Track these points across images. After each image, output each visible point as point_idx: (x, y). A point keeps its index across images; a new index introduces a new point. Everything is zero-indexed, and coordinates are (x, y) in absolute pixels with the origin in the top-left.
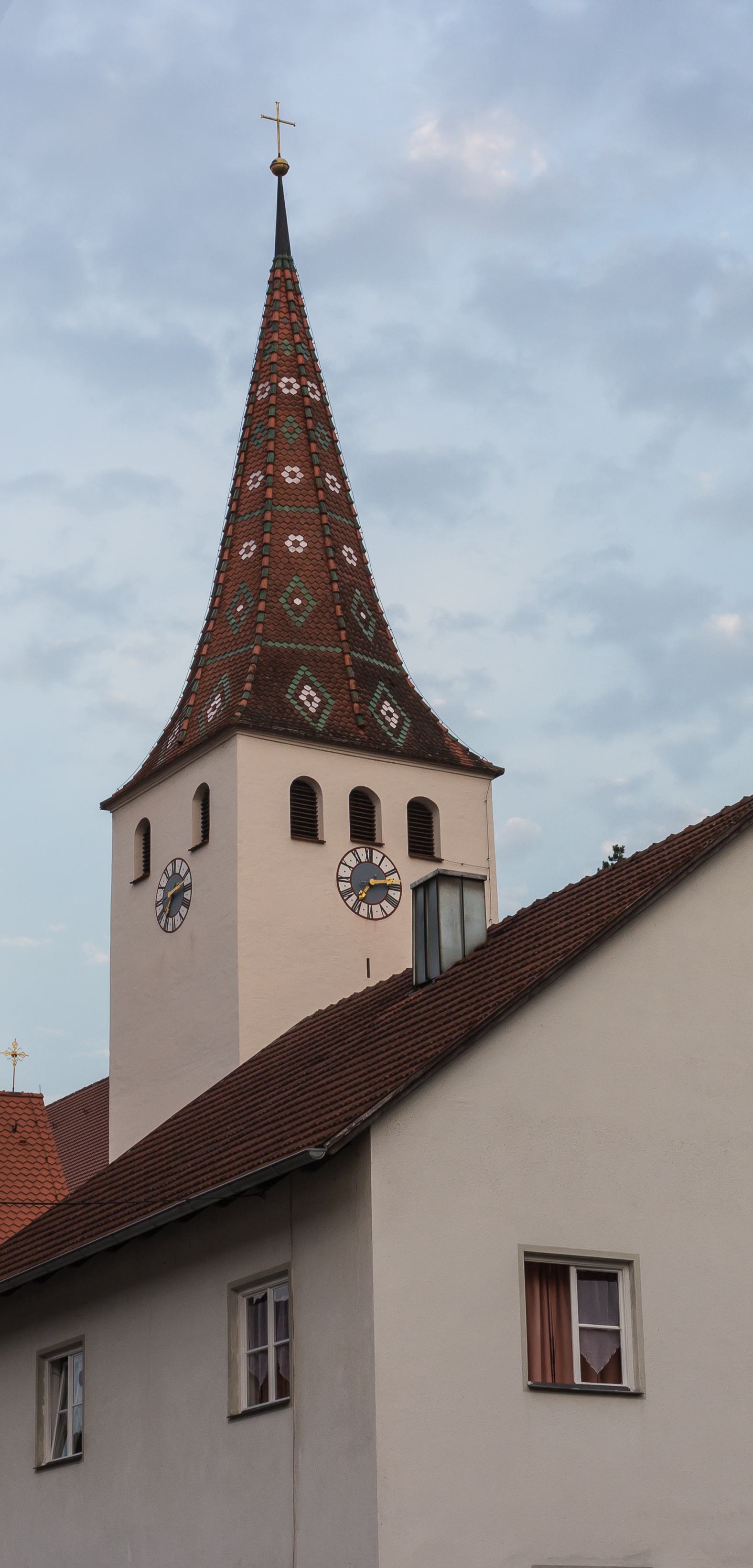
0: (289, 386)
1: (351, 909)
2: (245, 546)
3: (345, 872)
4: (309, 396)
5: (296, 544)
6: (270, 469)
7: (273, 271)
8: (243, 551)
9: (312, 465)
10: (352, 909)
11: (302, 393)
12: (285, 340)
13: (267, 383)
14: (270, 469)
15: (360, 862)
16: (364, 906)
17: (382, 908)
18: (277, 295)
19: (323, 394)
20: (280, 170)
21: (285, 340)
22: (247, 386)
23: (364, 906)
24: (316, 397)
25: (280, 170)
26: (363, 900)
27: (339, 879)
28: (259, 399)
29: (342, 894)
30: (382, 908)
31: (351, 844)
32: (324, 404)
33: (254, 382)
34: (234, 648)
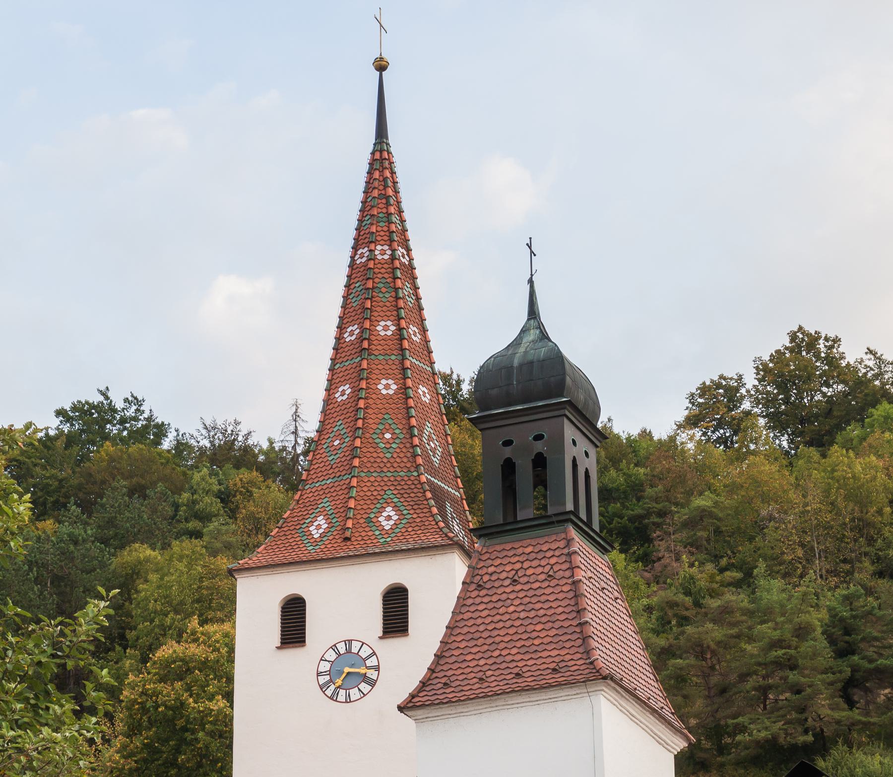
0: (382, 252)
1: (330, 698)
2: (340, 389)
4: (399, 260)
5: (387, 387)
6: (367, 324)
7: (373, 153)
8: (339, 394)
9: (399, 318)
10: (331, 698)
11: (393, 258)
12: (380, 211)
13: (366, 249)
14: (367, 324)
15: (339, 655)
17: (359, 690)
18: (377, 175)
19: (411, 259)
20: (381, 66)
21: (380, 211)
22: (348, 252)
24: (405, 261)
25: (381, 66)
26: (339, 687)
27: (319, 674)
28: (358, 262)
30: (359, 690)
31: (338, 635)
32: (412, 268)
33: (355, 248)
34: (321, 479)
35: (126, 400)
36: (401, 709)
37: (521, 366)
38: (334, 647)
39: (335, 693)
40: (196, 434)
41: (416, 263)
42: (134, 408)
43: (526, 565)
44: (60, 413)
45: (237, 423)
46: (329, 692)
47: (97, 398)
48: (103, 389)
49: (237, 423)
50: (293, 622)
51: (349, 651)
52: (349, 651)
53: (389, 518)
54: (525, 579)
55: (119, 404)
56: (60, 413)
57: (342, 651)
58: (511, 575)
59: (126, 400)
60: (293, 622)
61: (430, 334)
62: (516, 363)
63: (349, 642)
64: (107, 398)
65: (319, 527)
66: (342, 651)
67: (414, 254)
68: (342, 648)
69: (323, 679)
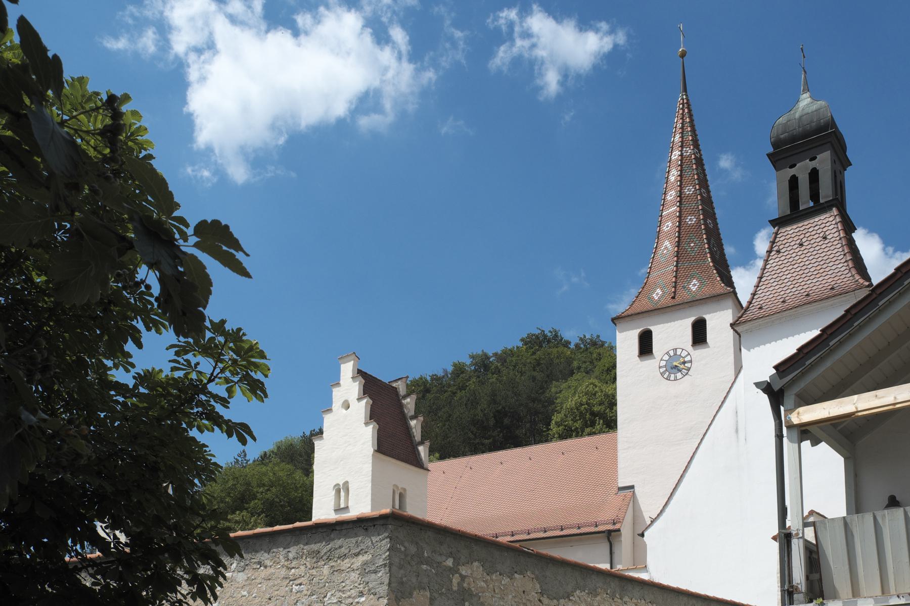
3: (663, 363)
19: (701, 155)
23: (672, 376)
27: (660, 367)
36: (770, 221)
38: (667, 353)
39: (669, 376)
41: (703, 157)
43: (807, 235)
44: (522, 340)
46: (665, 376)
50: (645, 345)
51: (675, 354)
52: (675, 354)
53: (695, 285)
54: (808, 243)
56: (522, 340)
58: (798, 242)
60: (645, 345)
61: (712, 194)
63: (675, 350)
65: (657, 294)
66: (678, 353)
67: (702, 152)
68: (672, 353)
69: (662, 370)
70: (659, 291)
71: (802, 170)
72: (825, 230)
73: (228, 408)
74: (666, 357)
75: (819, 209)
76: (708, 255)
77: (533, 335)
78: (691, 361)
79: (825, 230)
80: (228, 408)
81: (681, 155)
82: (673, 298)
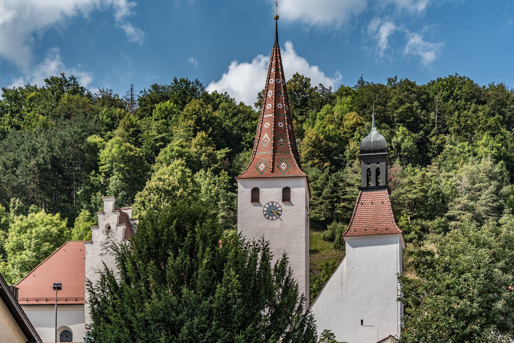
3: (265, 209)
16: (271, 217)
23: (271, 217)
27: (264, 211)
29: (264, 215)
35: (70, 78)
37: (373, 142)
38: (268, 204)
40: (97, 93)
42: (73, 81)
44: (47, 80)
45: (111, 90)
46: (267, 217)
47: (60, 76)
48: (62, 73)
49: (111, 90)
51: (273, 205)
52: (273, 205)
55: (68, 79)
56: (47, 80)
57: (279, 209)
59: (70, 78)
62: (372, 141)
63: (273, 202)
64: (64, 77)
66: (279, 209)
69: (265, 213)
70: (262, 165)
71: (373, 167)
72: (383, 199)
73: (175, 78)
74: (267, 206)
75: (378, 187)
76: (295, 160)
77: (297, 289)
78: (281, 211)
79: (383, 199)
80: (175, 78)
81: (276, 82)
82: (272, 172)
